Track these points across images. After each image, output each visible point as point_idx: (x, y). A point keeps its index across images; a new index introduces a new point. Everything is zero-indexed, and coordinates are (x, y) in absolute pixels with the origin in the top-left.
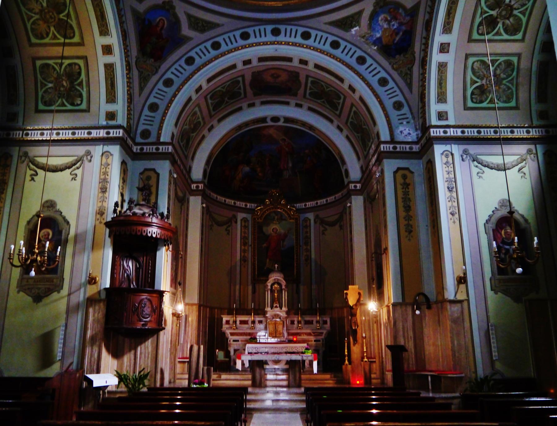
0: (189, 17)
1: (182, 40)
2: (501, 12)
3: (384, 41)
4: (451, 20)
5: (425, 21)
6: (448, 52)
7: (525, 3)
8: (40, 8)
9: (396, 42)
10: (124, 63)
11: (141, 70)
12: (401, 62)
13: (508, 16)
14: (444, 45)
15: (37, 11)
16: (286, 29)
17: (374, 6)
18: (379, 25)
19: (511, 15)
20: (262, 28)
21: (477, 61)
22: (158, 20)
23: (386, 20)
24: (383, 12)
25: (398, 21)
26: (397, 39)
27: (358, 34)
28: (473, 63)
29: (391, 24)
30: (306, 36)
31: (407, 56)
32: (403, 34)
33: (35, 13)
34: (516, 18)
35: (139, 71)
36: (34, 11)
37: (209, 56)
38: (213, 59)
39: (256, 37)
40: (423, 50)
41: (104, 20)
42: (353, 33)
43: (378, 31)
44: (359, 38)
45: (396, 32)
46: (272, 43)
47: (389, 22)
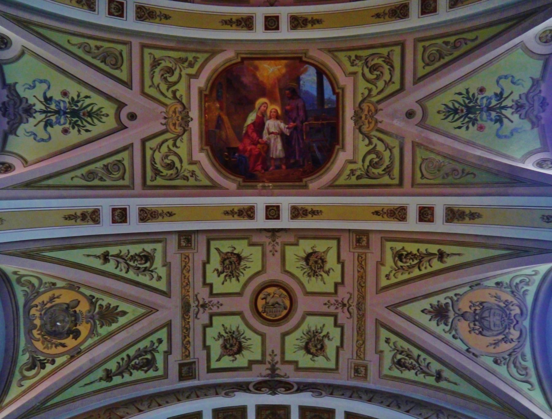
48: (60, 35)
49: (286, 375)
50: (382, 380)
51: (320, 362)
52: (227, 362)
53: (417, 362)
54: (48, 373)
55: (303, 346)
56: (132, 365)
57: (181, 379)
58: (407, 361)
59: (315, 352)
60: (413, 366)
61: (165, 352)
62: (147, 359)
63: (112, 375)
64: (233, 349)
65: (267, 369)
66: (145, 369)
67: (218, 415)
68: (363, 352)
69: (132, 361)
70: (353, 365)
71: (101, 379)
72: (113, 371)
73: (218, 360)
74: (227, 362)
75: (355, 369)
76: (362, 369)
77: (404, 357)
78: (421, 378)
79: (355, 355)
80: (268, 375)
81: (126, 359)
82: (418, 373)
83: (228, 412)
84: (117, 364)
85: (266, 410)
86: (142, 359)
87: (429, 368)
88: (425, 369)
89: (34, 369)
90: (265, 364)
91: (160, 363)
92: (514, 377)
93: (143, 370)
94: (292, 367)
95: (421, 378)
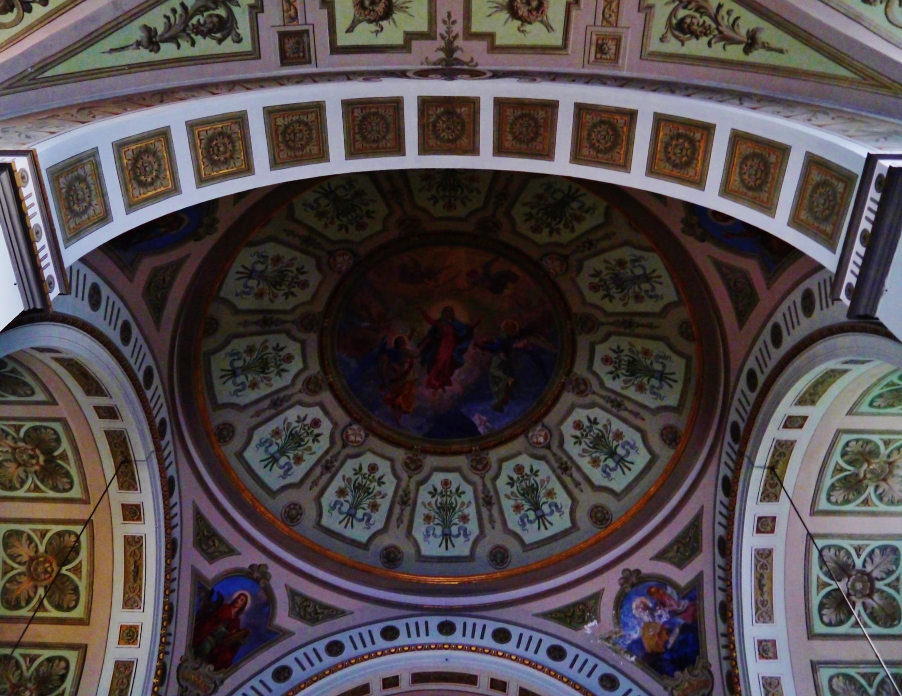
0: (293, 594)
1: (271, 635)
2: (853, 585)
3: (649, 645)
4: (766, 597)
5: (718, 605)
6: (772, 531)
7: (891, 569)
8: (32, 554)
9: (669, 646)
10: (155, 663)
11: (184, 684)
12: (686, 685)
13: (868, 592)
14: (764, 643)
15: (25, 558)
16: (465, 624)
17: (622, 585)
18: (634, 616)
19: (872, 591)
20: (421, 620)
21: (838, 675)
22: (236, 595)
23: (646, 608)
24: (639, 595)
25: (667, 609)
26: (672, 640)
27: (598, 635)
28: (831, 680)
29: (656, 614)
30: (502, 636)
31: (696, 672)
32: (681, 632)
33: (20, 563)
34: (885, 595)
35: (180, 685)
36: (18, 560)
37: (319, 666)
38: (327, 672)
39: (409, 636)
40: (726, 658)
41: (138, 581)
42: (589, 631)
43: (634, 628)
44: (599, 642)
45: (668, 629)
46: (439, 647)
47: (652, 611)
48: (195, 484)
49: (472, 60)
50: (646, 62)
51: (536, 34)
52: (364, 34)
53: (715, 20)
54: (38, 20)
55: (505, 4)
56: (193, 25)
57: (285, 61)
58: (695, 21)
59: (526, 14)
60: (705, 28)
61: (251, 7)
62: (218, 16)
63: (158, 39)
64: (377, 9)
65: (439, 49)
66: (218, 35)
67: (353, 113)
68: (615, 10)
69: (191, 18)
70: (594, 38)
71: (138, 44)
72: (160, 32)
73: (350, 30)
74: (364, 34)
75: (597, 44)
76: (611, 45)
77: (691, 13)
78: (718, 51)
79: (600, 16)
80: (440, 61)
81: (179, 10)
82: (713, 41)
83: (370, 108)
84: (165, 20)
85: (437, 107)
86: (211, 16)
87: (736, 27)
88: (728, 32)
89: (12, 11)
90: (435, 38)
91: (243, 26)
92: (895, 22)
93: (214, 38)
94: (483, 45)
95: (718, 51)
